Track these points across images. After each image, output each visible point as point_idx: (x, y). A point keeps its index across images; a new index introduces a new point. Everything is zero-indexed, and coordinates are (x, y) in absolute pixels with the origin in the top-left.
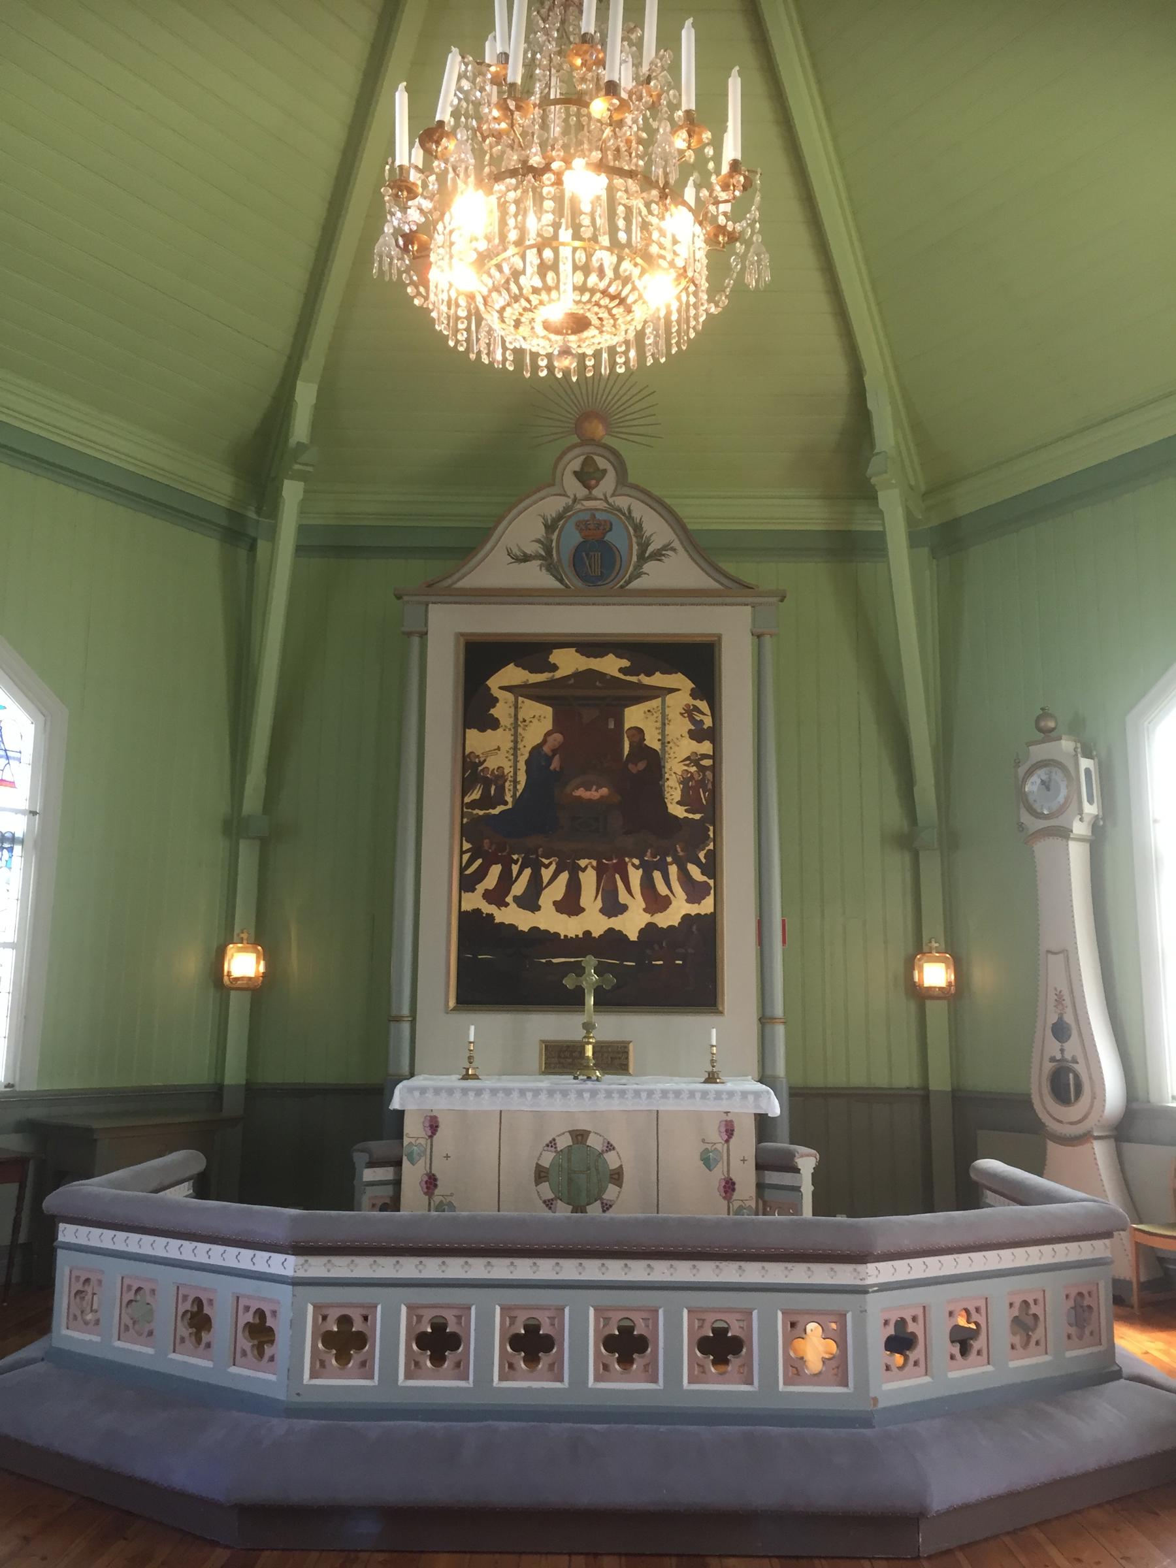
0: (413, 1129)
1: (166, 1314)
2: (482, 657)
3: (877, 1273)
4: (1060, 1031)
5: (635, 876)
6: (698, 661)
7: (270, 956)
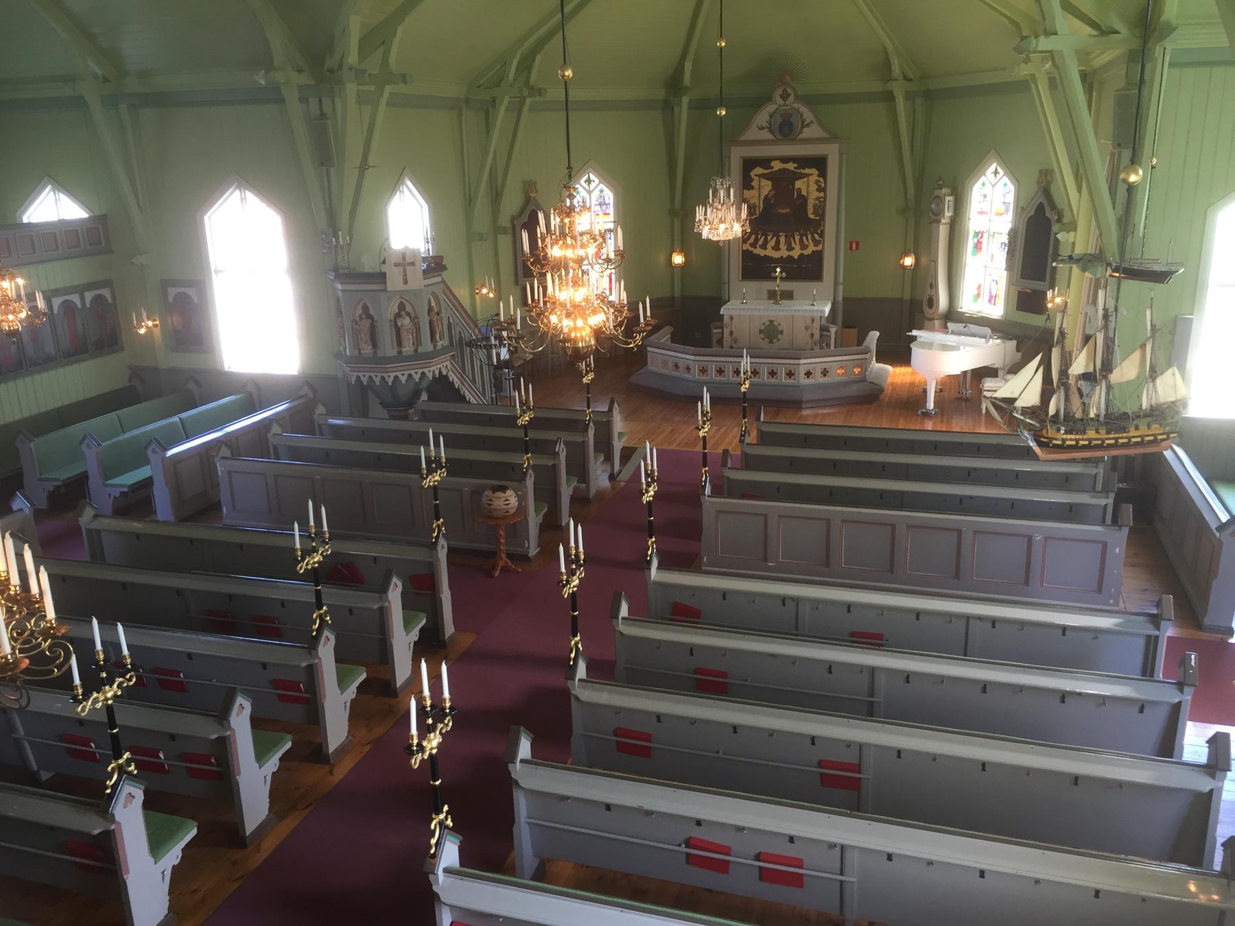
0: (726, 319)
1: (671, 365)
2: (749, 164)
3: (803, 361)
4: (931, 286)
5: (797, 238)
6: (820, 163)
7: (686, 256)
